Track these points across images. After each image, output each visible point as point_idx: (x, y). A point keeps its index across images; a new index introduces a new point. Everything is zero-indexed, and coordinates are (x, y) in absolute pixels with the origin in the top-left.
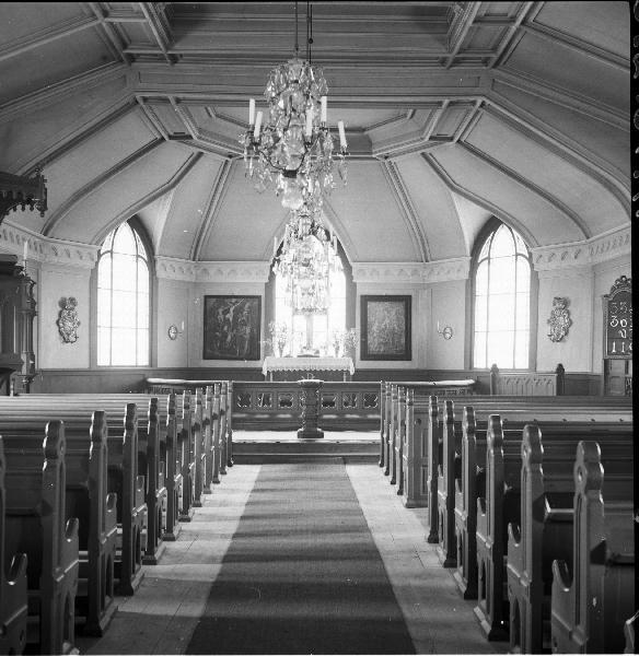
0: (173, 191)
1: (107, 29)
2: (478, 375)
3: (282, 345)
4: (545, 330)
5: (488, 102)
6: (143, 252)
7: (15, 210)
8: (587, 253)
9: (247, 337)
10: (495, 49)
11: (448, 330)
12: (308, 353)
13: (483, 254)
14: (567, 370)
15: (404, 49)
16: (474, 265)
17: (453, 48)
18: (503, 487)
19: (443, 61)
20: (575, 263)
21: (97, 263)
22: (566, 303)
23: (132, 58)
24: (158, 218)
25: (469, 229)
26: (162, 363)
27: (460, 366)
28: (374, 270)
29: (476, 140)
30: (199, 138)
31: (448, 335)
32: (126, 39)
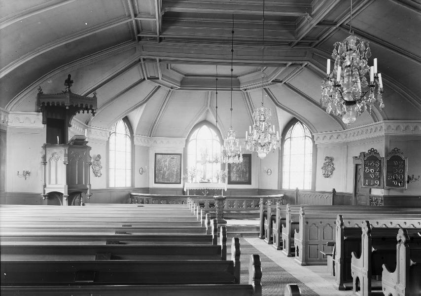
0: (145, 104)
1: (134, 21)
2: (284, 191)
3: (192, 177)
4: (320, 172)
5: (310, 64)
6: (129, 133)
7: (79, 113)
8: (344, 136)
9: (175, 173)
10: (318, 39)
11: (269, 171)
12: (204, 181)
13: (288, 135)
14: (337, 191)
15: (280, 37)
16: (283, 140)
17: (299, 38)
18: (410, 262)
19: (290, 44)
20: (337, 141)
21: (109, 138)
22: (332, 159)
23: (140, 39)
24: (136, 117)
25: (282, 124)
26: (137, 185)
27: (275, 187)
28: (101, 132)
29: (293, 83)
30: (162, 79)
31: (269, 173)
32: (140, 28)
